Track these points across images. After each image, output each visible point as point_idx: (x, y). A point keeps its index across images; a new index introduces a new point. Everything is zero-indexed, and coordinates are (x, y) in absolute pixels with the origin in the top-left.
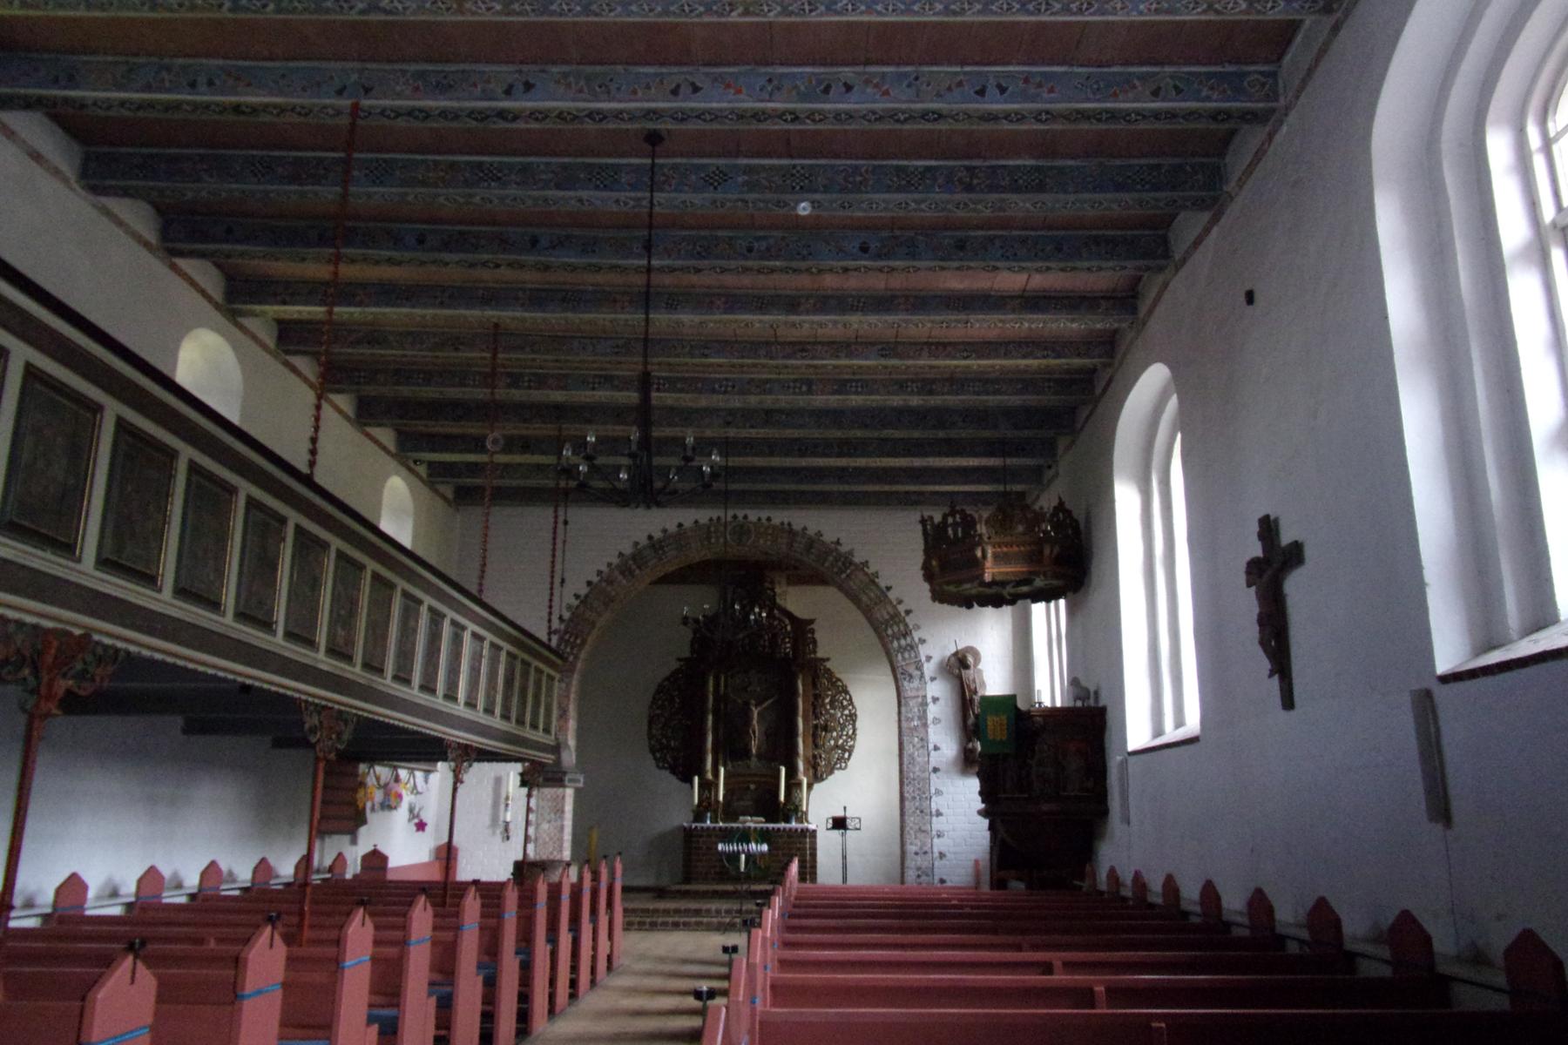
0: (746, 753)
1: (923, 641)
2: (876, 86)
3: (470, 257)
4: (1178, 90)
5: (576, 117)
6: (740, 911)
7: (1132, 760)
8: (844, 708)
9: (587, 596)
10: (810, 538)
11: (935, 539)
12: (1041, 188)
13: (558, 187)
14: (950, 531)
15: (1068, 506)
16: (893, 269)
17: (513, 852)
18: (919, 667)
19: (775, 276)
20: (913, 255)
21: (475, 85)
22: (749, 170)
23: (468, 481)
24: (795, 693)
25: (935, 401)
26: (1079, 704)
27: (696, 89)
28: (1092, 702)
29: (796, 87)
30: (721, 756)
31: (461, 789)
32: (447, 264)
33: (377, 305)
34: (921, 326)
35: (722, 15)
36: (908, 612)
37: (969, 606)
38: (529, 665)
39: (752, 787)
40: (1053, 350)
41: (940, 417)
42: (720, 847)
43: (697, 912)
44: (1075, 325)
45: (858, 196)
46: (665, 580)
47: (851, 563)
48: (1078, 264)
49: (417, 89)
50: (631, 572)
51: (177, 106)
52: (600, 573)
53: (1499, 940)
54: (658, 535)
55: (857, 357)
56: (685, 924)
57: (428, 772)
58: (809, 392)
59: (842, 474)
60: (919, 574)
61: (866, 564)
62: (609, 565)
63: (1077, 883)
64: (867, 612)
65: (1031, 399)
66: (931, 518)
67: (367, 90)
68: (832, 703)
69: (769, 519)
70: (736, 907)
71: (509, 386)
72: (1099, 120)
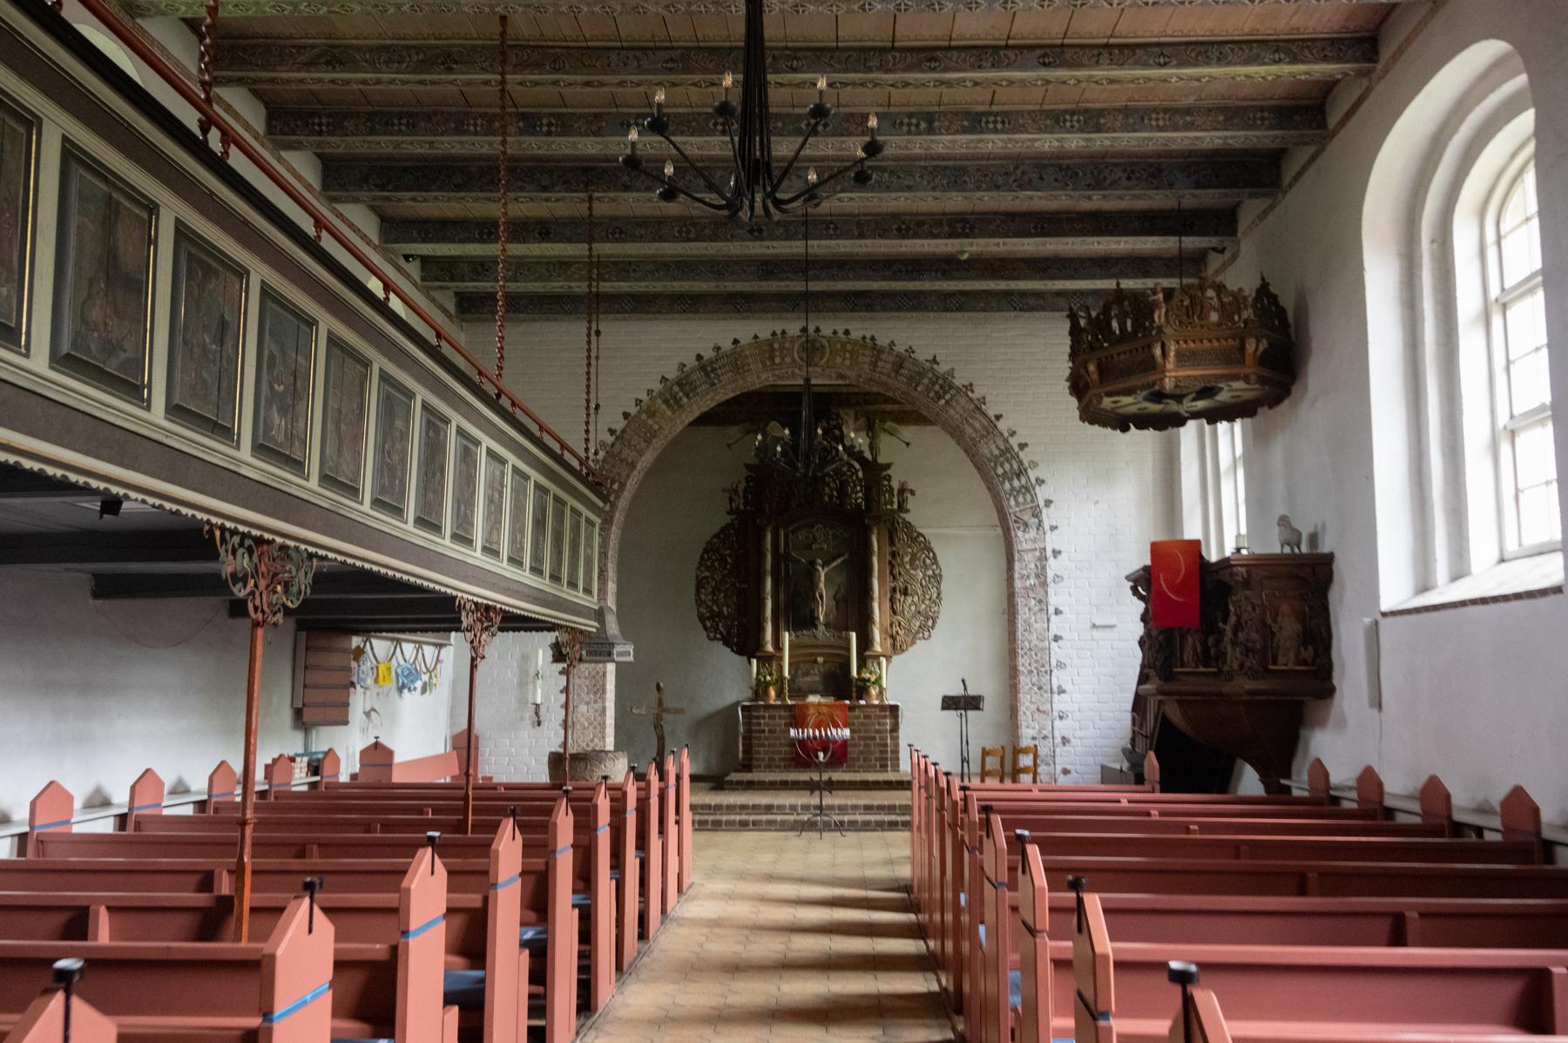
0: (811, 622)
1: (1040, 482)
6: (820, 808)
7: (1383, 622)
8: (926, 567)
9: (623, 431)
14: (1115, 324)
15: (1272, 289)
17: (551, 739)
18: (1036, 514)
23: (469, 286)
24: (868, 546)
25: (1101, 141)
26: (1287, 550)
28: (1304, 549)
30: (782, 625)
31: (481, 665)
36: (1022, 446)
37: (1125, 429)
38: (564, 503)
39: (820, 660)
40: (1288, 52)
42: (793, 732)
43: (769, 809)
46: (705, 419)
47: (951, 387)
50: (678, 401)
52: (638, 402)
53: (1497, 795)
54: (708, 354)
55: (1009, 66)
56: (754, 823)
57: (440, 646)
58: (930, 131)
60: (1064, 386)
62: (650, 392)
63: (1283, 782)
64: (971, 452)
65: (1210, 138)
68: (912, 562)
69: (847, 332)
71: (522, 132)
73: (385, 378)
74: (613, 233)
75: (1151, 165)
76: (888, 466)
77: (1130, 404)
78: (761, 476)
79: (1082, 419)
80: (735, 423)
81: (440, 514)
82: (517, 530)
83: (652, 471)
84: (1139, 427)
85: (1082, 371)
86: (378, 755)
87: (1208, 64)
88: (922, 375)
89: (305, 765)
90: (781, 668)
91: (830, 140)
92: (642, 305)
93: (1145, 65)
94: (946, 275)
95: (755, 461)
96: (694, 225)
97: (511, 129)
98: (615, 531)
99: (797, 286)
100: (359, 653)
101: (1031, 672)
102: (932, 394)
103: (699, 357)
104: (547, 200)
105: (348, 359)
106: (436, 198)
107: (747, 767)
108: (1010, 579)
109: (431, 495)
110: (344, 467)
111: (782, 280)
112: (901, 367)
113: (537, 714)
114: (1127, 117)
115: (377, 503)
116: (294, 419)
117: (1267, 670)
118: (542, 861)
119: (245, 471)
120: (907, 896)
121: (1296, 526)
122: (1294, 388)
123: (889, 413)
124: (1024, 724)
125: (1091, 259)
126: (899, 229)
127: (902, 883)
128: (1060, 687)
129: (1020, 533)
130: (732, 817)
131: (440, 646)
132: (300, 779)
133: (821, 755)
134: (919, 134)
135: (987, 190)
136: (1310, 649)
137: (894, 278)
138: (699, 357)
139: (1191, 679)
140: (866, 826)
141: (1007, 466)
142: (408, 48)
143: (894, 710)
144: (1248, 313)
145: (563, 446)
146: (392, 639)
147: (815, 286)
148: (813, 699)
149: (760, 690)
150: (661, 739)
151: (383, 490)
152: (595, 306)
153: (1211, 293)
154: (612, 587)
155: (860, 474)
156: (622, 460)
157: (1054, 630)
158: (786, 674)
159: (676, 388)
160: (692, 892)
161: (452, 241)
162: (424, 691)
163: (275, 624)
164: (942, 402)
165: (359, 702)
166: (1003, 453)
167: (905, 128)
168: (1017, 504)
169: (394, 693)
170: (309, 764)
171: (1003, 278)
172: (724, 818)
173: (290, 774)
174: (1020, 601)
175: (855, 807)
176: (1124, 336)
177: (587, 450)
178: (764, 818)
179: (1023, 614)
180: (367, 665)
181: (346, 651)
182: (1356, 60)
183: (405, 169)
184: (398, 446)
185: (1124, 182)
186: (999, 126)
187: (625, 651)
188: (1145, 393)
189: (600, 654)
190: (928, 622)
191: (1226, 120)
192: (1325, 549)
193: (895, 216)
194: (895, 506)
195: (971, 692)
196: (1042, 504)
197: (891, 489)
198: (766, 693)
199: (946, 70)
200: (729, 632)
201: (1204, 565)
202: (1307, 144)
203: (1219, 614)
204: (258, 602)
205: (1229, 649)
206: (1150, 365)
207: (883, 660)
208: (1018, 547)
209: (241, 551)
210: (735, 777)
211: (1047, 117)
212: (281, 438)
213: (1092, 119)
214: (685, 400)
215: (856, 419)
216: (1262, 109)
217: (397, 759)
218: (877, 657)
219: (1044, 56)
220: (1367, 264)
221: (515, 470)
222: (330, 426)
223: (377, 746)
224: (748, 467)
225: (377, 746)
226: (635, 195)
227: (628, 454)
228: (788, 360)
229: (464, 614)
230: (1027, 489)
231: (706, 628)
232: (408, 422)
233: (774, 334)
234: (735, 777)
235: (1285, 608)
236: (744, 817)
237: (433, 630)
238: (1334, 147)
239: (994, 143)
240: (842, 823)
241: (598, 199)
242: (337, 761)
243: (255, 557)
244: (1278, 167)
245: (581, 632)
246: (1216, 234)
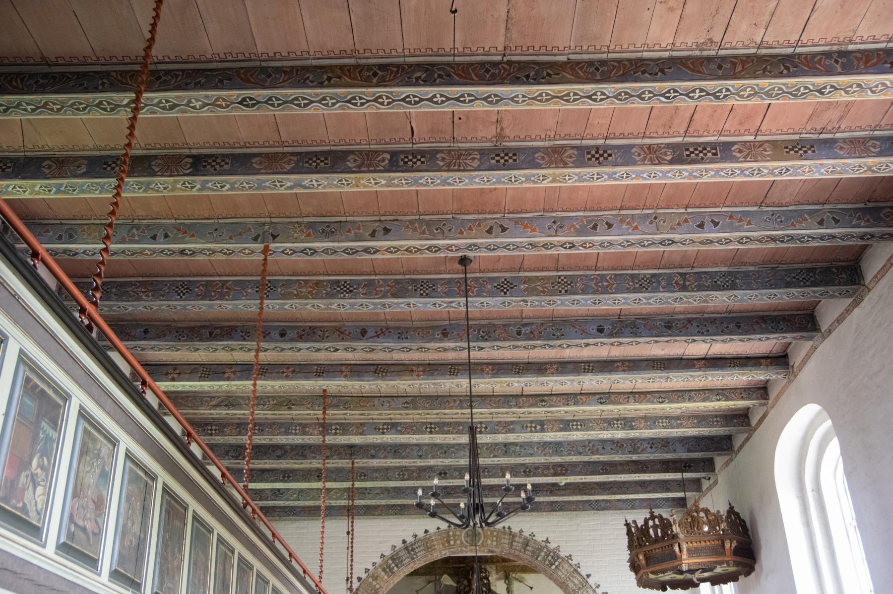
2: (628, 223)
3: (317, 345)
4: (837, 221)
5: (419, 250)
9: (357, 589)
10: (526, 538)
11: (637, 538)
12: (734, 287)
13: (394, 296)
14: (651, 531)
15: (736, 509)
16: (621, 343)
19: (536, 350)
20: (636, 335)
21: (349, 231)
22: (528, 280)
25: (633, 434)
27: (504, 229)
29: (573, 226)
32: (300, 349)
33: (240, 379)
34: (624, 382)
35: (536, 182)
37: (664, 589)
40: (724, 395)
41: (634, 445)
44: (744, 378)
45: (606, 296)
46: (416, 573)
47: (558, 558)
48: (753, 337)
49: (309, 235)
50: (391, 570)
51: (142, 252)
52: (367, 570)
54: (410, 539)
58: (542, 430)
61: (570, 557)
65: (705, 431)
66: (635, 522)
67: (274, 237)
72: (782, 241)
74: (360, 476)
85: (636, 559)
87: (684, 401)
88: (540, 550)
91: (488, 436)
92: (370, 511)
93: (653, 402)
94: (552, 493)
102: (547, 562)
103: (404, 542)
112: (527, 545)
114: (646, 421)
122: (756, 566)
126: (525, 472)
134: (537, 432)
135: (574, 455)
138: (404, 542)
142: (269, 397)
153: (702, 514)
159: (390, 562)
161: (267, 481)
164: (554, 567)
167: (529, 429)
171: (585, 494)
176: (657, 540)
182: (758, 399)
185: (649, 450)
191: (698, 422)
199: (550, 406)
206: (673, 557)
211: (605, 422)
213: (628, 423)
214: (396, 569)
216: (716, 416)
219: (600, 398)
228: (458, 542)
246: (704, 471)
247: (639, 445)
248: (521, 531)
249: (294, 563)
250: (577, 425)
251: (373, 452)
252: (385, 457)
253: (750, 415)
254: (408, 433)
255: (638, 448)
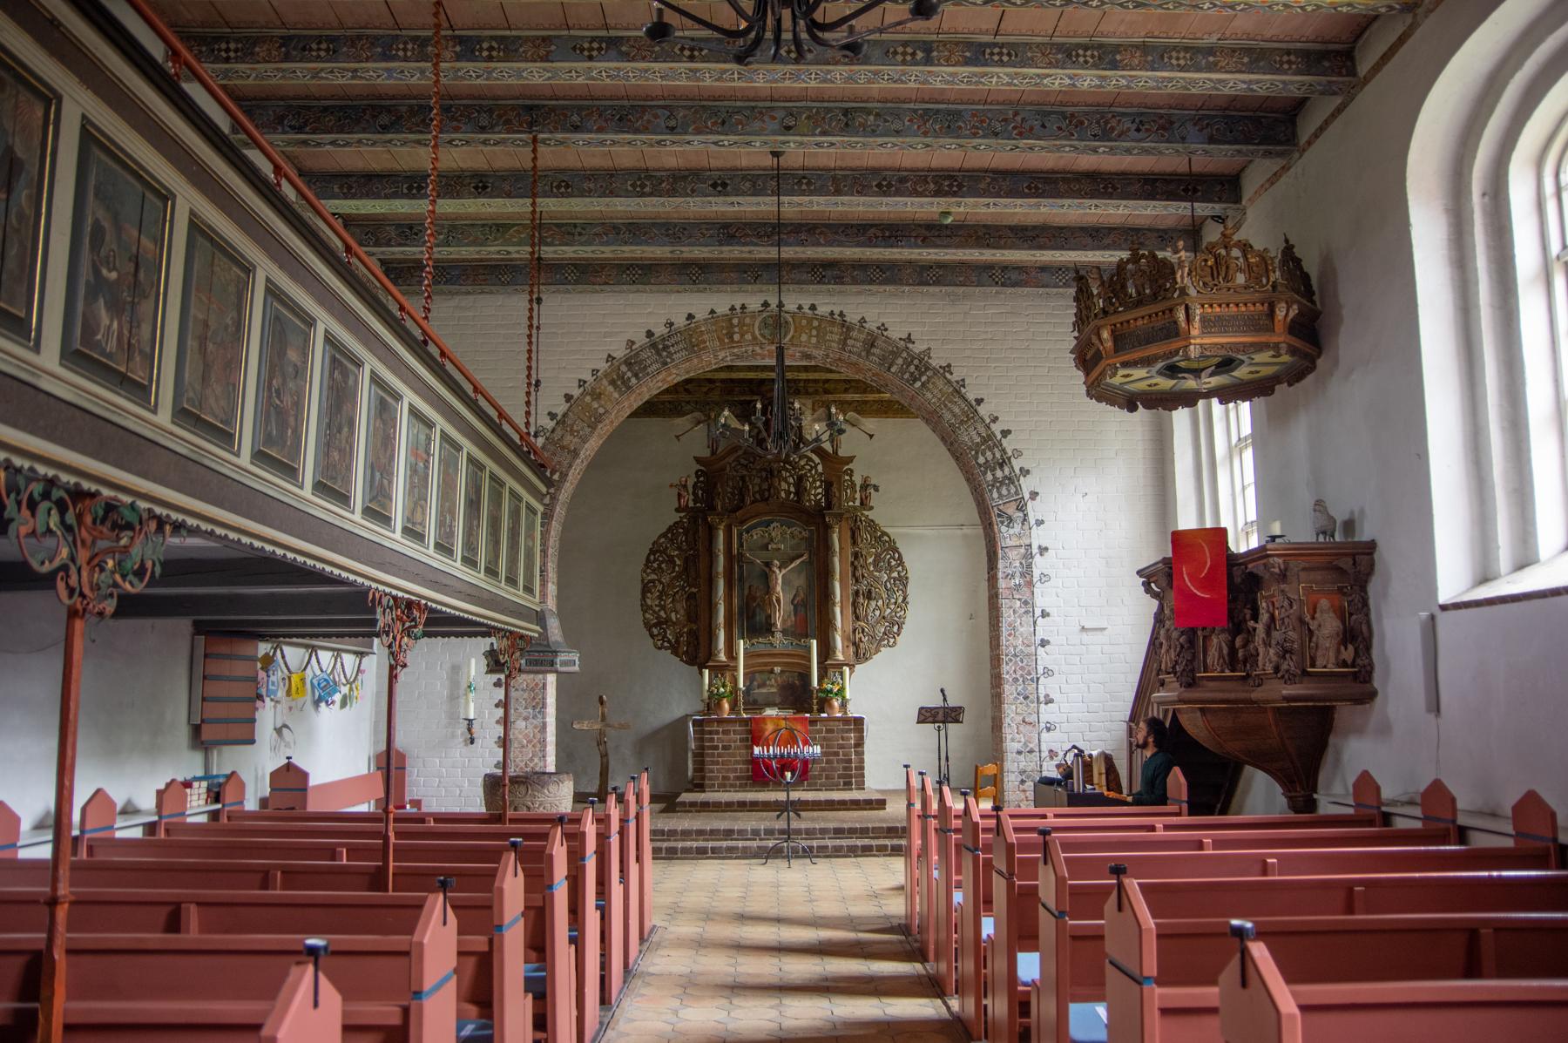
0: (767, 629)
1: (1025, 472)
8: (891, 569)
9: (565, 415)
15: (1297, 252)
17: (487, 758)
18: (1021, 508)
23: (396, 252)
24: (828, 547)
25: (1116, 80)
26: (1321, 539)
30: (736, 631)
31: (403, 675)
36: (1005, 433)
37: (1132, 408)
39: (777, 669)
42: (757, 750)
43: (728, 834)
46: (649, 409)
47: (927, 369)
50: (626, 382)
52: (582, 383)
54: (660, 330)
56: (714, 850)
57: (361, 654)
58: (928, 61)
59: (931, 232)
61: (948, 368)
62: (595, 372)
65: (1233, 82)
68: (876, 563)
69: (813, 307)
70: (781, 824)
73: (273, 291)
74: (558, 187)
75: (1161, 116)
76: (851, 459)
77: (1140, 378)
78: (709, 475)
79: (1089, 394)
80: (681, 414)
81: (347, 480)
82: (446, 511)
83: (594, 465)
84: (1147, 407)
85: (1094, 339)
86: (290, 779)
88: (896, 354)
89: (203, 790)
90: (735, 680)
92: (586, 274)
94: (926, 242)
95: (706, 453)
96: (649, 178)
97: (448, 54)
98: (556, 527)
99: (767, 252)
100: (268, 661)
101: (1015, 680)
102: (906, 376)
103: (650, 334)
104: (485, 142)
105: (218, 254)
106: (360, 141)
107: (700, 787)
108: (992, 579)
109: (336, 455)
110: (212, 401)
111: (745, 244)
112: (872, 345)
113: (469, 730)
115: (259, 456)
116: (134, 324)
117: (1305, 673)
118: (483, 939)
119: (46, 384)
120: (906, 939)
121: (1332, 513)
122: (1321, 362)
123: (850, 403)
124: (1009, 737)
125: (1082, 229)
126: (879, 186)
127: (895, 922)
128: (1047, 696)
129: (1004, 529)
130: (688, 844)
131: (361, 654)
132: (197, 808)
133: (788, 775)
135: (984, 137)
136: (1351, 648)
137: (870, 243)
138: (650, 334)
139: (1211, 684)
140: (837, 853)
141: (989, 455)
143: (859, 722)
144: (1276, 276)
145: (501, 415)
146: (306, 646)
147: (789, 252)
148: (771, 712)
149: (713, 704)
150: (604, 756)
151: (269, 440)
152: (537, 275)
153: (1236, 252)
154: (552, 588)
155: (820, 468)
156: (563, 448)
157: (1040, 634)
158: (741, 685)
159: (624, 368)
160: (655, 938)
162: (344, 704)
163: (101, 614)
164: (918, 384)
165: (267, 717)
166: (985, 441)
167: (899, 58)
168: (1001, 496)
169: (309, 706)
170: (209, 790)
172: (680, 845)
173: (183, 800)
174: (1004, 603)
175: (823, 831)
177: (527, 424)
178: (724, 844)
179: (1007, 616)
180: (277, 676)
181: (254, 659)
183: (326, 109)
184: (291, 385)
185: (1133, 134)
186: (1005, 58)
187: (570, 660)
188: (1160, 365)
189: (541, 663)
190: (894, 626)
191: (1251, 62)
192: (1365, 534)
193: (875, 171)
194: (858, 503)
195: (952, 703)
196: (1027, 496)
197: (853, 485)
198: (719, 705)
200: (677, 641)
201: (1233, 560)
202: (1335, 93)
203: (1248, 613)
204: (73, 581)
205: (1261, 650)
206: (1172, 331)
207: (846, 669)
208: (1001, 543)
209: (45, 505)
210: (686, 797)
212: (112, 346)
214: (634, 381)
215: (814, 410)
216: (1288, 52)
217: (313, 782)
218: (840, 666)
220: (1413, 220)
221: (445, 437)
222: (191, 343)
223: (289, 767)
224: (698, 460)
225: (289, 767)
226: (586, 136)
227: (569, 440)
228: (748, 337)
229: (379, 610)
230: (1010, 480)
231: (652, 636)
232: (305, 355)
233: (733, 309)
234: (686, 797)
235: (1324, 603)
236: (701, 844)
237: (350, 635)
238: (1367, 98)
239: (999, 79)
240: (811, 848)
241: (544, 141)
242: (241, 786)
243: (70, 518)
244: (1294, 124)
245: (522, 637)
246: (1220, 200)
247: (1113, 123)
248: (863, 321)
249: (449, 367)
250: (1001, 54)
251: (575, 118)
252: (600, 130)
253: (1357, 54)
254: (644, 59)
255: (1113, 129)
